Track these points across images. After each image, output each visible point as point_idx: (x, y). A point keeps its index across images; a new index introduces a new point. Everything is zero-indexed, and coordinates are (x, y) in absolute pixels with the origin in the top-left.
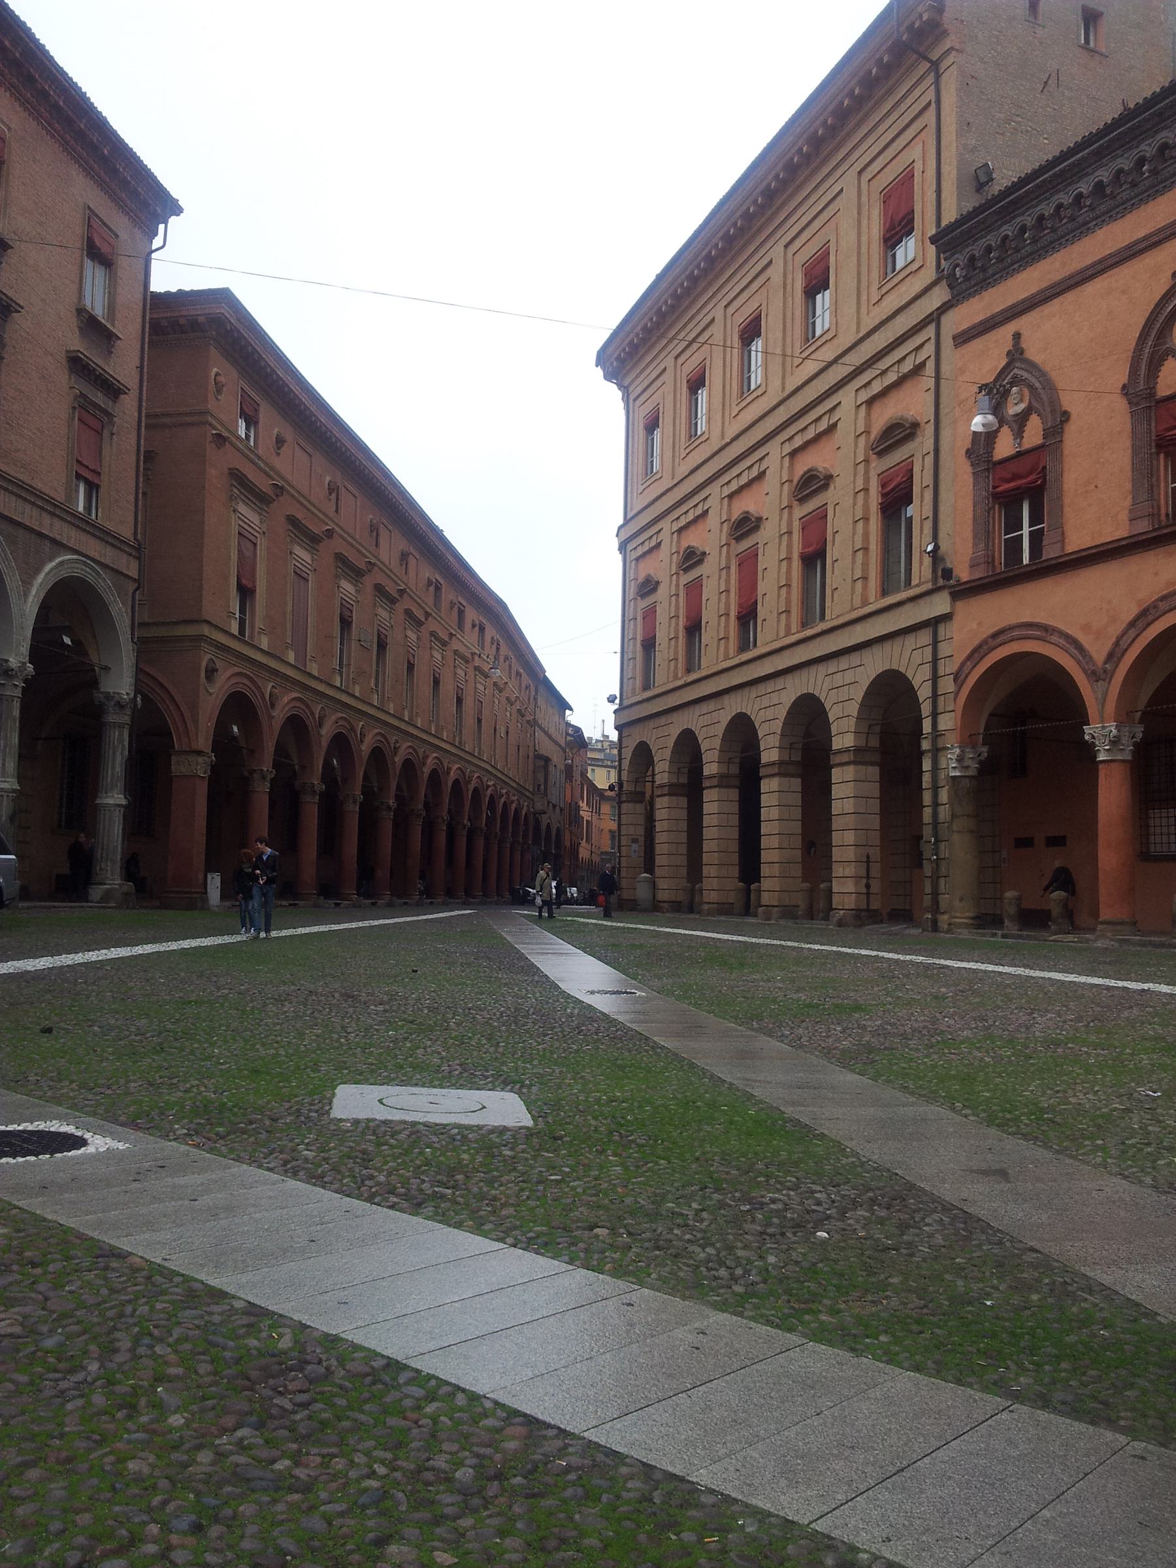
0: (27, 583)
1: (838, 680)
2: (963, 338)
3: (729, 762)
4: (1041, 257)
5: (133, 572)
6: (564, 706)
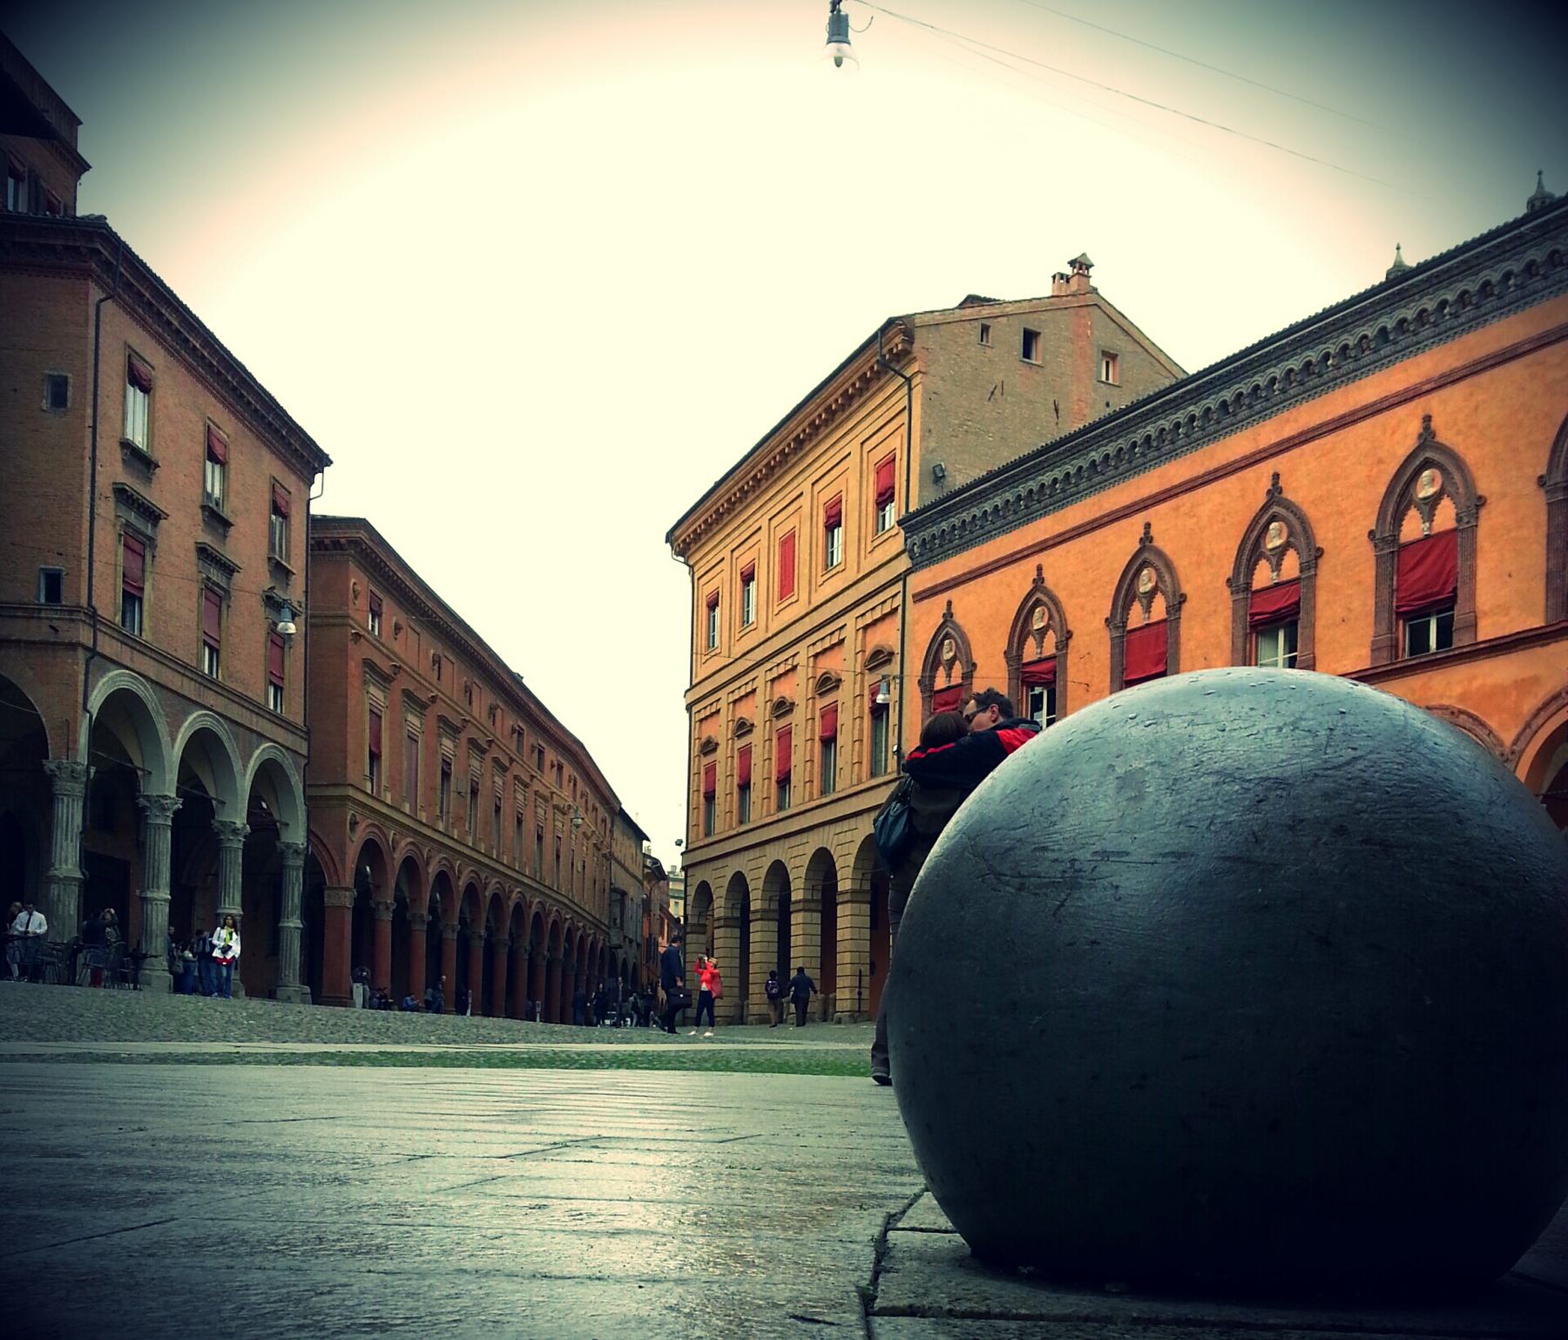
0: (246, 758)
1: (795, 852)
2: (920, 597)
3: (770, 899)
4: (964, 549)
5: (305, 752)
6: (641, 836)
